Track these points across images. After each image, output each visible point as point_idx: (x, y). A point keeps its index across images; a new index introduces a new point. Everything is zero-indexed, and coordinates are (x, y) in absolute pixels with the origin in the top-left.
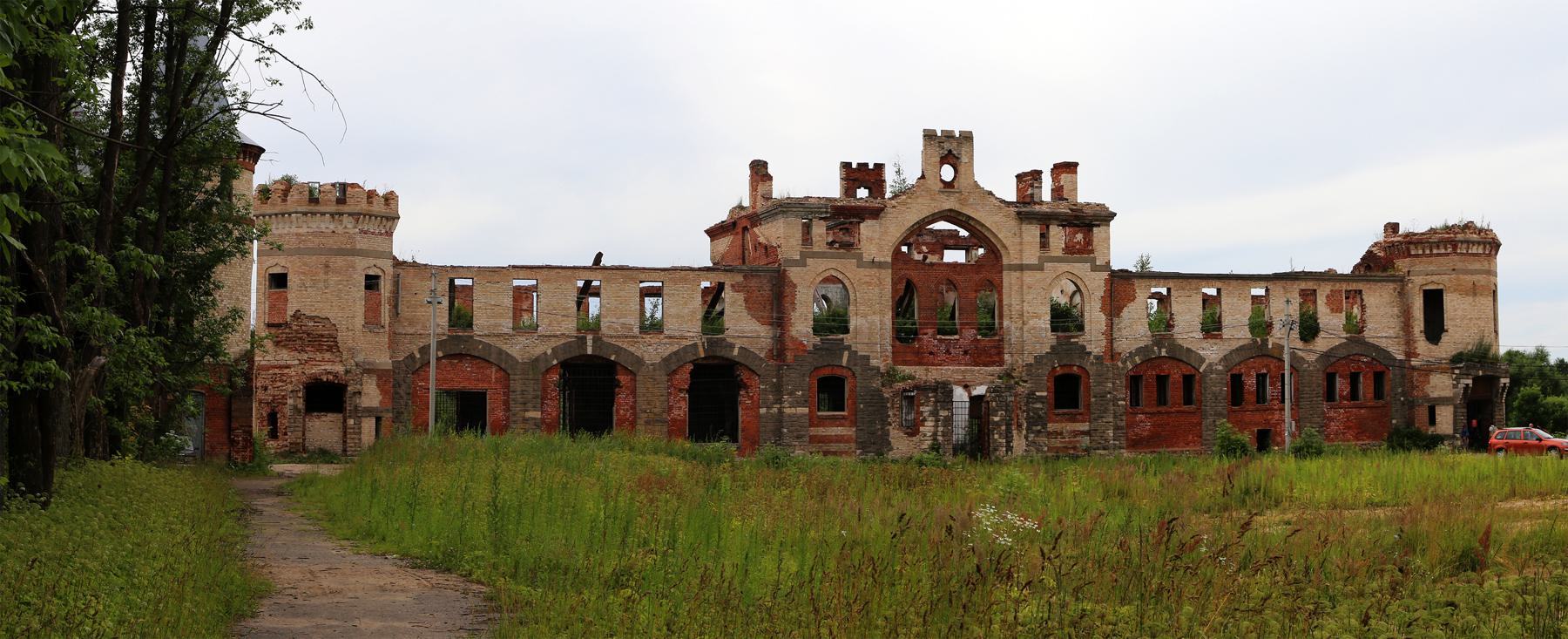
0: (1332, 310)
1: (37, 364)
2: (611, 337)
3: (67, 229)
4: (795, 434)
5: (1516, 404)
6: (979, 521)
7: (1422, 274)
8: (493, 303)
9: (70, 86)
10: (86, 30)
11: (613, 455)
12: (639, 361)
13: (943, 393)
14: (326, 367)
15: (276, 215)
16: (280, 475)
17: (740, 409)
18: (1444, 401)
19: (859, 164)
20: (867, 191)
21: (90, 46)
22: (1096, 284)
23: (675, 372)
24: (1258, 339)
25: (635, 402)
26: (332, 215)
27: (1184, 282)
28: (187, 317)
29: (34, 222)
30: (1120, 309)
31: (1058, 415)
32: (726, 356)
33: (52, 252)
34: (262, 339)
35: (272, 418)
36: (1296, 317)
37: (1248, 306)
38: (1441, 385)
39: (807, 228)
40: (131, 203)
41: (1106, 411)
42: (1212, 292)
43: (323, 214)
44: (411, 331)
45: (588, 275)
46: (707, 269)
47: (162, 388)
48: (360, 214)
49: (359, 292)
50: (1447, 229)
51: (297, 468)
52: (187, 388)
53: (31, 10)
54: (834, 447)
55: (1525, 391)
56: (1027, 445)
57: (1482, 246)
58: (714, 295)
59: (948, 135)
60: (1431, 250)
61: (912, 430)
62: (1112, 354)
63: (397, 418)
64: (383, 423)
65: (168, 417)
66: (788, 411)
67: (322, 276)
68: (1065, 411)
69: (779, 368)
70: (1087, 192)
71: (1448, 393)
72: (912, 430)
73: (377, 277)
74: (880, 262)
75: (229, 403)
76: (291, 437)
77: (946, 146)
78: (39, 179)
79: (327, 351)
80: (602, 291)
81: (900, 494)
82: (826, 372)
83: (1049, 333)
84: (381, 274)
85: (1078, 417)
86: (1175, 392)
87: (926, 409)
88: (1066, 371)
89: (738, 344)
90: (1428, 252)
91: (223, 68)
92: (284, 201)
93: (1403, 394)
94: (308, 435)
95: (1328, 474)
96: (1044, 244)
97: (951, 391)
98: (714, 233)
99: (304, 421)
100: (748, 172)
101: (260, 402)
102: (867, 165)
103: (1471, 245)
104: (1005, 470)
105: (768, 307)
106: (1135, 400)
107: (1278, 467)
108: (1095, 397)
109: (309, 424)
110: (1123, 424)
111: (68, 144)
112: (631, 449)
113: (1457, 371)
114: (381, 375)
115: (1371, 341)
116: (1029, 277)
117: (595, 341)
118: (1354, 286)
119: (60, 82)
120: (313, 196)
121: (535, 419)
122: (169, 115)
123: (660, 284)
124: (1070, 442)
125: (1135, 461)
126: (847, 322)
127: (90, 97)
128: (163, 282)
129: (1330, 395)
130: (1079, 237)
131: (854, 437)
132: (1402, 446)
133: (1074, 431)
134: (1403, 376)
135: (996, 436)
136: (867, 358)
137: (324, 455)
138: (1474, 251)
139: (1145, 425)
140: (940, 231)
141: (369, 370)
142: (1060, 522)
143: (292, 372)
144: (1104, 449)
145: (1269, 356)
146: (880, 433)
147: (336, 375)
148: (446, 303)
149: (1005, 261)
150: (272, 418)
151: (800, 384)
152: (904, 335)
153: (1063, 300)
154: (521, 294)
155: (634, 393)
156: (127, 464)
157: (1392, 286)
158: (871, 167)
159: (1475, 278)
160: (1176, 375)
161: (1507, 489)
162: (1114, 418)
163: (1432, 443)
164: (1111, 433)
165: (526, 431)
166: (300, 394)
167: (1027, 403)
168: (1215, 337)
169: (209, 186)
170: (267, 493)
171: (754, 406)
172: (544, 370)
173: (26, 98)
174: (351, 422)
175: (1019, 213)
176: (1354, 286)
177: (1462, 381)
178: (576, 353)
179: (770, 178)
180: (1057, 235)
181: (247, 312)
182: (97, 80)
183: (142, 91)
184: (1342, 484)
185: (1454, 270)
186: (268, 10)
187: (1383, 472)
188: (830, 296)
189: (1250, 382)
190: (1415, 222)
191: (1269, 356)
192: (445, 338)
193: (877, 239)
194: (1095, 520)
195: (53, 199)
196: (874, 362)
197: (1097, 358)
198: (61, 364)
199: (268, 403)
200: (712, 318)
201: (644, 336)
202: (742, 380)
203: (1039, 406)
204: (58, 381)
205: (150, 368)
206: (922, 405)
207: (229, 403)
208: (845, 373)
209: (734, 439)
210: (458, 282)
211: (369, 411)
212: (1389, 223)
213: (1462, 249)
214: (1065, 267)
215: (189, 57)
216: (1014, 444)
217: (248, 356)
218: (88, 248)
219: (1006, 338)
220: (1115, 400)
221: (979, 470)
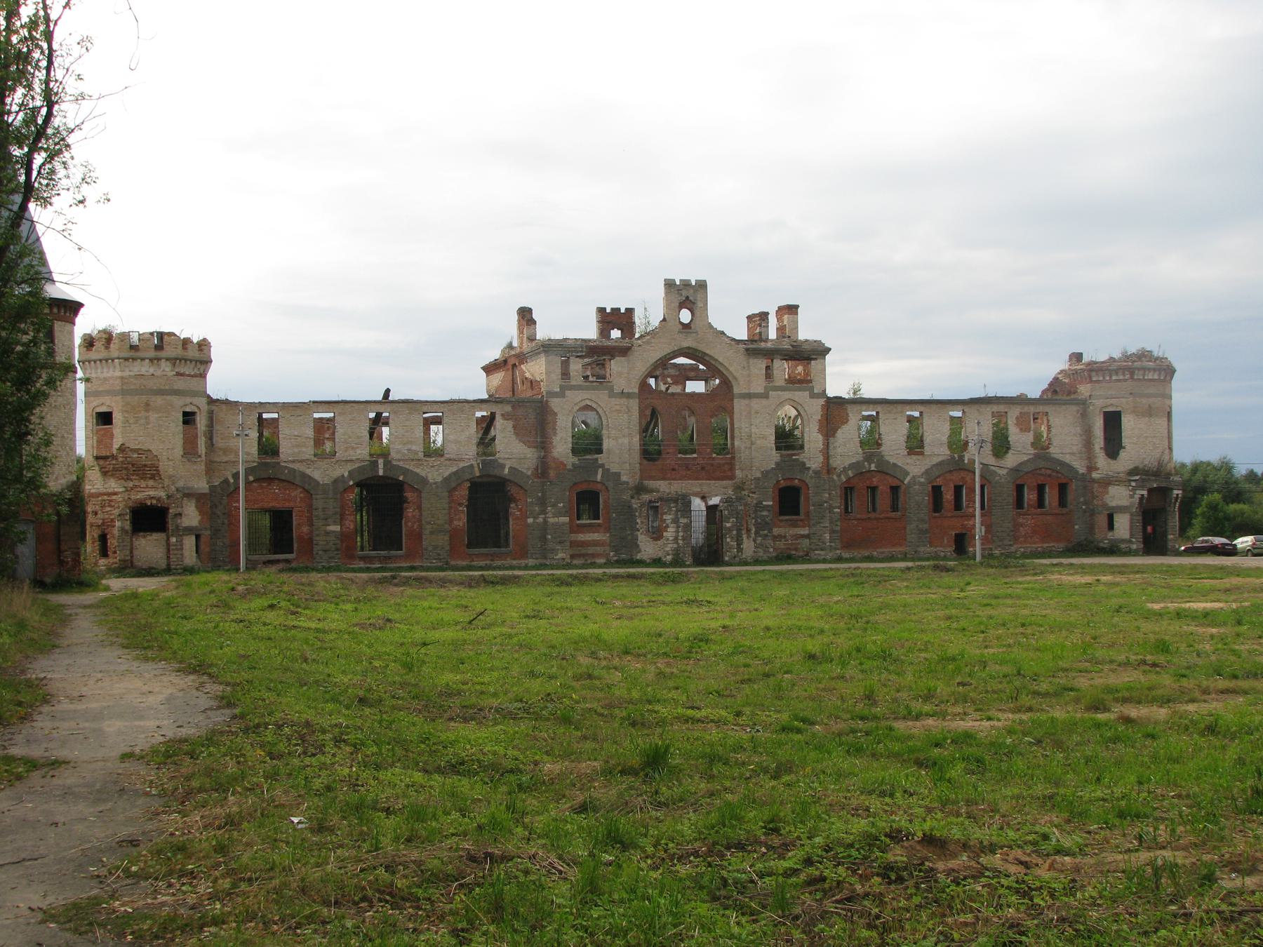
0: (1021, 429)
2: (399, 460)
4: (558, 540)
8: (296, 433)
12: (424, 481)
14: (149, 493)
15: (101, 360)
17: (511, 520)
19: (612, 309)
20: (620, 331)
22: (815, 409)
23: (455, 489)
24: (956, 456)
25: (421, 515)
26: (151, 360)
31: (781, 521)
32: (498, 474)
35: (103, 538)
38: (1119, 496)
39: (565, 364)
41: (823, 517)
43: (143, 359)
44: (225, 459)
45: (380, 408)
46: (482, 401)
48: (176, 359)
56: (756, 547)
57: (1157, 373)
58: (487, 424)
59: (686, 284)
60: (1111, 377)
61: (657, 534)
62: (829, 470)
66: (551, 520)
68: (787, 517)
70: (806, 332)
71: (1125, 502)
72: (657, 534)
73: (193, 414)
74: (628, 393)
79: (151, 478)
80: (391, 421)
82: (584, 487)
83: (774, 452)
84: (196, 410)
85: (799, 522)
86: (883, 500)
88: (789, 483)
89: (508, 464)
90: (1108, 378)
92: (107, 348)
93: (1085, 503)
94: (135, 552)
96: (769, 374)
97: (690, 502)
98: (489, 369)
99: (132, 541)
100: (516, 317)
101: (92, 526)
102: (619, 309)
103: (1147, 372)
105: (534, 433)
108: (813, 505)
109: (136, 543)
110: (838, 528)
113: (1133, 484)
114: (200, 498)
115: (1056, 456)
116: (756, 404)
121: (334, 532)
123: (441, 414)
124: (792, 544)
126: (601, 444)
129: (1019, 503)
130: (800, 369)
131: (608, 541)
133: (796, 535)
134: (1085, 487)
135: (728, 540)
138: (1150, 377)
140: (683, 364)
141: (189, 494)
144: (822, 550)
145: (966, 470)
146: (630, 537)
147: (159, 499)
149: (736, 390)
150: (103, 538)
152: (650, 454)
154: (321, 426)
155: (419, 508)
157: (1075, 408)
158: (623, 311)
159: (1151, 400)
160: (883, 489)
162: (830, 523)
164: (827, 536)
166: (128, 517)
167: (756, 511)
172: (342, 490)
174: (173, 540)
175: (747, 350)
176: (1041, 408)
177: (1138, 492)
179: (534, 322)
185: (1131, 394)
188: (589, 421)
189: (948, 496)
191: (966, 470)
192: (255, 464)
193: (623, 373)
196: (624, 478)
197: (816, 472)
199: (99, 526)
201: (428, 459)
202: (512, 495)
203: (765, 513)
206: (665, 513)
208: (599, 486)
211: (189, 530)
212: (1073, 353)
214: (787, 395)
216: (744, 546)
219: (737, 455)
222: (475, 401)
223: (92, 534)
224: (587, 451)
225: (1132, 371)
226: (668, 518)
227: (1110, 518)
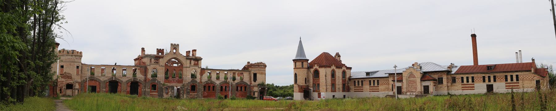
1: (22, 81)
3: (27, 57)
5: (268, 92)
6: (178, 108)
7: (253, 71)
9: (26, 32)
10: (29, 23)
11: (117, 97)
12: (122, 81)
13: (172, 88)
14: (70, 81)
16: (62, 99)
18: (256, 91)
21: (29, 26)
22: (199, 70)
23: (128, 83)
27: (213, 71)
28: (47, 73)
29: (21, 56)
30: (203, 75)
33: (24, 61)
34: (59, 77)
35: (61, 90)
36: (232, 77)
37: (224, 75)
38: (256, 89)
39: (151, 60)
40: (37, 53)
42: (218, 72)
43: (70, 55)
46: (134, 66)
47: (42, 85)
50: (258, 63)
51: (65, 98)
52: (46, 85)
53: (19, 19)
54: (154, 96)
55: (270, 90)
58: (135, 70)
59: (175, 45)
61: (167, 93)
62: (201, 82)
63: (81, 90)
65: (43, 90)
66: (147, 90)
67: (69, 66)
70: (198, 55)
71: (257, 90)
72: (167, 93)
73: (79, 66)
75: (54, 87)
76: (64, 93)
78: (22, 49)
81: (165, 104)
86: (211, 88)
87: (170, 90)
91: (52, 30)
95: (236, 103)
96: (190, 63)
98: (135, 60)
100: (141, 50)
104: (182, 100)
106: (205, 90)
107: (228, 101)
111: (26, 43)
112: (120, 96)
114: (79, 83)
115: (245, 81)
116: (188, 69)
117: (115, 78)
118: (242, 72)
119: (25, 32)
120: (68, 52)
122: (44, 38)
125: (204, 100)
127: (30, 34)
128: (43, 67)
129: (237, 90)
130: (196, 62)
132: (249, 98)
134: (249, 87)
136: (160, 82)
137: (69, 96)
139: (206, 94)
142: (191, 109)
147: (71, 83)
148: (90, 71)
149: (184, 66)
150: (61, 90)
151: (149, 86)
152: (166, 78)
153: (193, 73)
154: (103, 70)
155: (121, 86)
156: (36, 97)
157: (248, 72)
160: (212, 86)
161: (266, 106)
163: (254, 98)
165: (103, 92)
166: (65, 86)
168: (218, 80)
169: (50, 50)
170: (59, 102)
171: (141, 89)
173: (19, 35)
176: (242, 72)
178: (112, 80)
179: (145, 51)
180: (193, 62)
181: (57, 72)
182: (31, 31)
183: (39, 33)
184: (238, 104)
186: (60, 20)
187: (246, 102)
189: (224, 87)
190: (253, 62)
193: (162, 62)
194: (197, 109)
195: (24, 52)
196: (161, 82)
197: (198, 83)
198: (26, 81)
200: (134, 74)
204: (25, 84)
205: (41, 81)
207: (54, 87)
209: (137, 94)
210: (92, 67)
211: (77, 89)
213: (260, 67)
214: (194, 67)
215: (46, 28)
216: (184, 96)
217: (57, 80)
218: (30, 60)
220: (201, 90)
221: (178, 100)
222: (133, 66)
223: (58, 89)
224: (154, 77)
225: (259, 66)
226: (170, 90)
227: (254, 93)
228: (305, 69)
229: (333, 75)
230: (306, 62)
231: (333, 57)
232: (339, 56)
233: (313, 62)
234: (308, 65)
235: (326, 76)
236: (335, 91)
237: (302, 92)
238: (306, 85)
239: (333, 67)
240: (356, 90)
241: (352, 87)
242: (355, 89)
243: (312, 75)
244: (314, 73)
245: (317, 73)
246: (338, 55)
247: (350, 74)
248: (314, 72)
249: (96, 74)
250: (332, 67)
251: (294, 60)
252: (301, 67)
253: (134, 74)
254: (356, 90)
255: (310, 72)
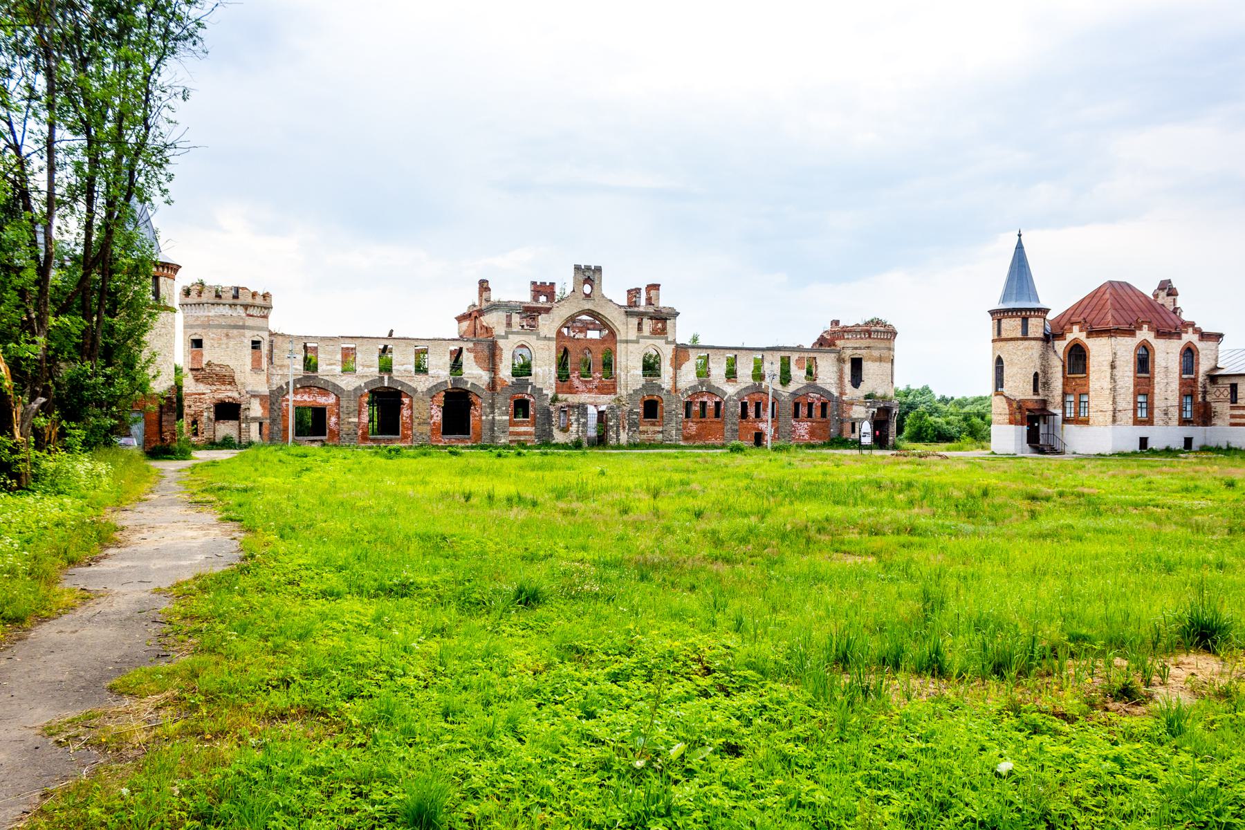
12: (415, 390)
13: (582, 409)
14: (227, 394)
18: (862, 420)
22: (667, 352)
26: (230, 305)
27: (717, 351)
30: (681, 365)
38: (858, 412)
39: (509, 317)
45: (386, 342)
49: (248, 350)
59: (588, 268)
64: (264, 426)
69: (493, 394)
71: (863, 416)
76: (206, 435)
77: (587, 274)
88: (651, 398)
93: (838, 415)
96: (640, 329)
98: (460, 319)
109: (218, 427)
114: (262, 398)
116: (631, 347)
117: (390, 378)
118: (812, 355)
129: (796, 415)
130: (660, 325)
136: (542, 389)
143: (206, 397)
149: (618, 338)
155: (411, 407)
157: (833, 355)
160: (711, 405)
164: (674, 432)
171: (478, 416)
176: (812, 355)
180: (648, 325)
193: (548, 325)
197: (668, 391)
200: (456, 366)
210: (308, 345)
211: (255, 419)
214: (651, 342)
216: (621, 437)
226: (573, 418)
227: (853, 425)
228: (1033, 342)
229: (1144, 362)
230: (1040, 317)
231: (1146, 297)
232: (1172, 293)
233: (1067, 317)
234: (1045, 329)
235: (1113, 367)
236: (1149, 421)
237: (1022, 424)
238: (1036, 397)
239: (1145, 334)
240: (1238, 421)
241: (1223, 408)
242: (1233, 416)
243: (1060, 364)
244: (1070, 356)
245: (1078, 358)
246: (1167, 288)
247: (1216, 359)
248: (1071, 349)
249: (323, 369)
250: (1137, 332)
251: (992, 313)
252: (1019, 335)
253: (456, 366)
254: (1238, 421)
255: (1052, 353)
